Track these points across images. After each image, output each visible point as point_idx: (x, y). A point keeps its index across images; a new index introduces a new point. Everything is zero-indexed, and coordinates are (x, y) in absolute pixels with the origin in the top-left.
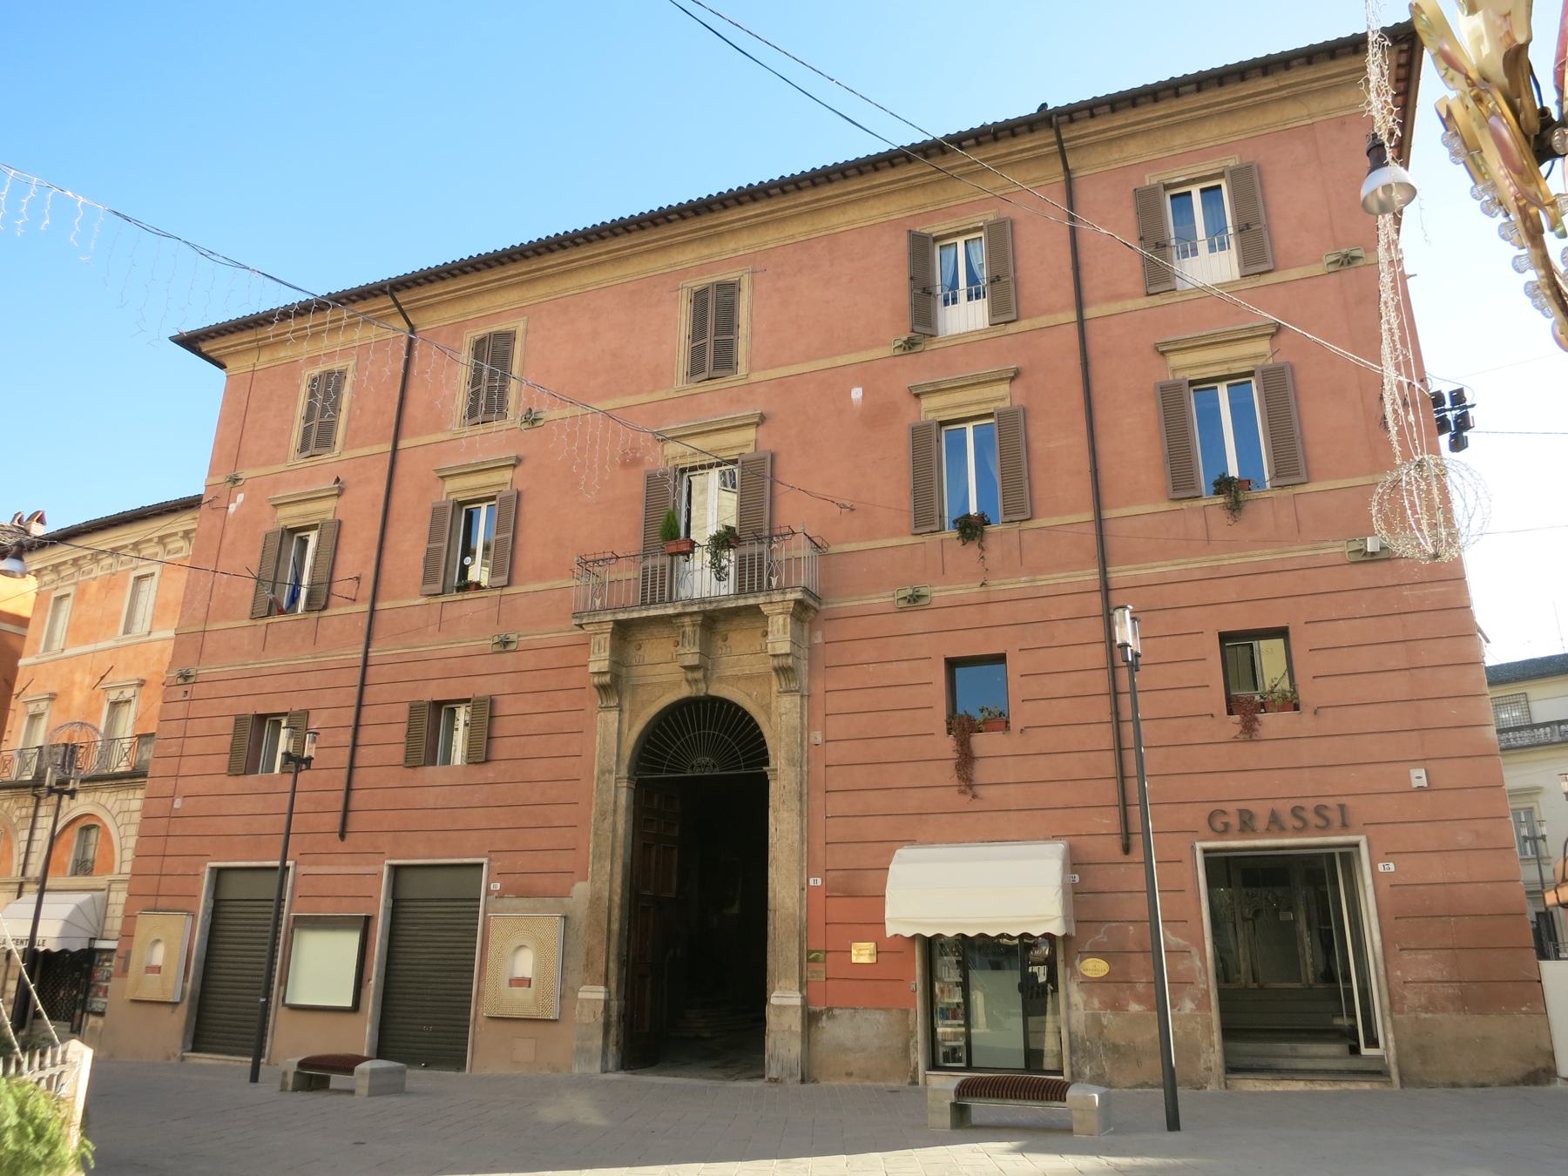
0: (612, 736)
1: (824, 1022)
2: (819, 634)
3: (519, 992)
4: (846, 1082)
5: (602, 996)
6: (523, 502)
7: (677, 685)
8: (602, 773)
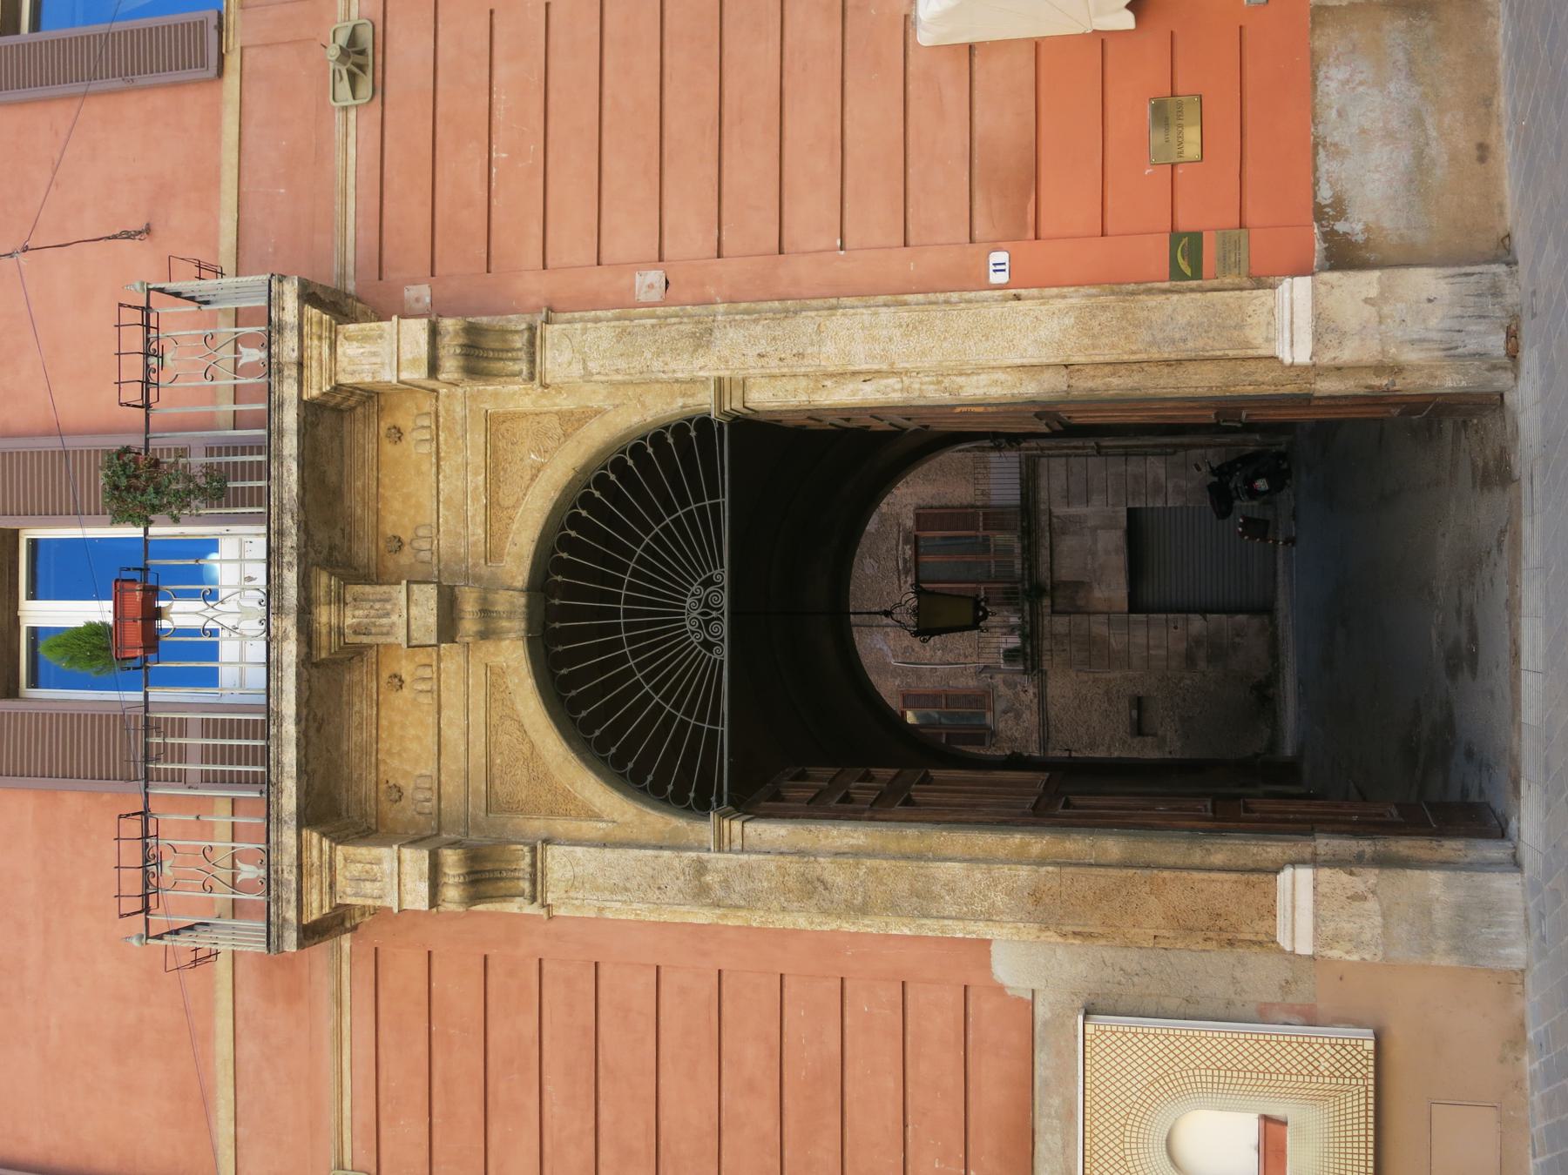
0: (622, 873)
1: (1353, 226)
2: (411, 292)
4: (1506, 152)
5: (1305, 875)
8: (701, 893)
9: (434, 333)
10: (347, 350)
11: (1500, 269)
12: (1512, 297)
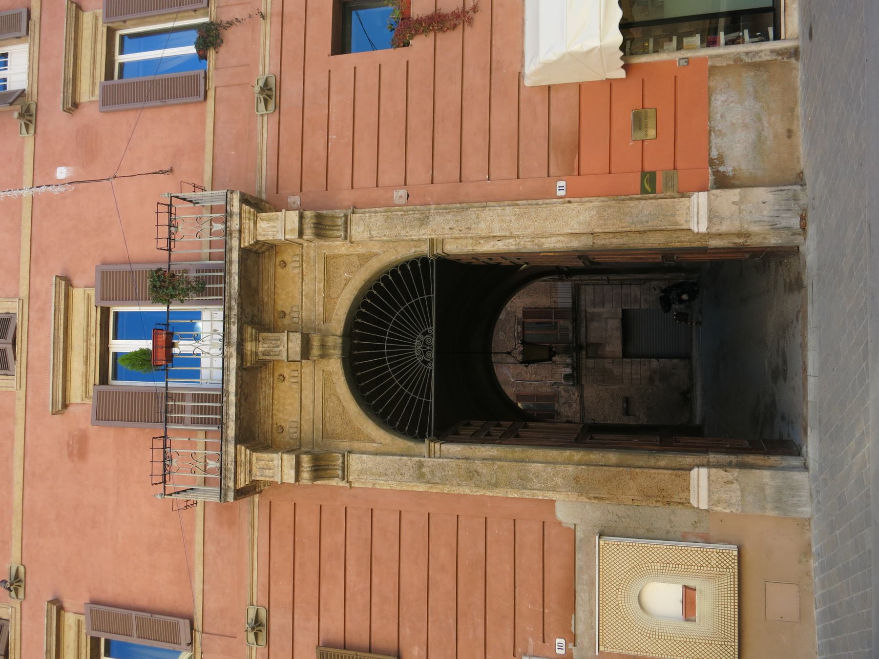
0: (382, 466)
1: (727, 168)
3: (703, 605)
4: (801, 133)
5: (704, 471)
6: (103, 597)
7: (327, 377)
8: (421, 477)
9: (301, 217)
10: (262, 225)
11: (798, 188)
12: (803, 200)
